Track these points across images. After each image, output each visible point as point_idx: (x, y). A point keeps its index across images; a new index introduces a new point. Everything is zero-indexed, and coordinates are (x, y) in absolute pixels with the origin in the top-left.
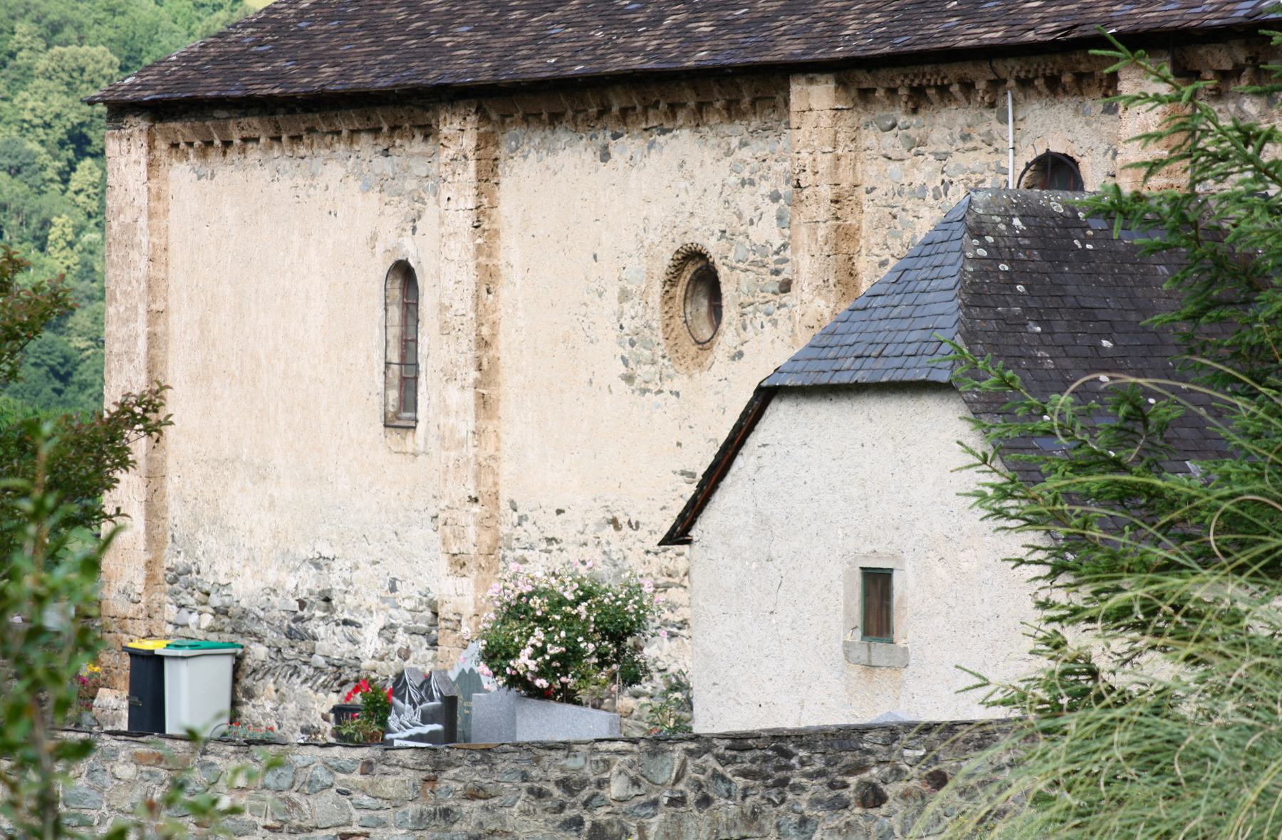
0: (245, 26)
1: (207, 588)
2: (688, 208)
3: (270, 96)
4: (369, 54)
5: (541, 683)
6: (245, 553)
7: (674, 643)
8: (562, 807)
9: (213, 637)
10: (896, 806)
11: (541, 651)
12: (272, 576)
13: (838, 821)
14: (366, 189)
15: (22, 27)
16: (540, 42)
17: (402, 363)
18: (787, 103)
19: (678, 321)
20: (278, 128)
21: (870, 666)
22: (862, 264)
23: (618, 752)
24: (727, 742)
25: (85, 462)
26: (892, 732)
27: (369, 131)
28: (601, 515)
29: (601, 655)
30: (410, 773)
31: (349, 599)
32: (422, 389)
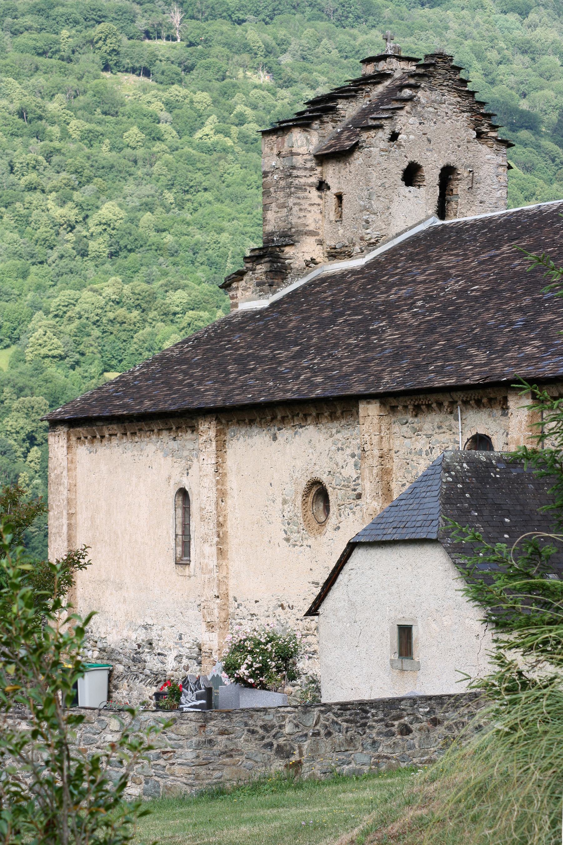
0: (110, 384)
1: (96, 639)
2: (313, 461)
3: (122, 415)
4: (166, 395)
5: (251, 681)
6: (113, 623)
7: (311, 661)
8: (263, 738)
9: (99, 662)
10: (416, 734)
11: (250, 666)
12: (125, 634)
13: (390, 742)
14: (166, 456)
15: (7, 389)
16: (244, 387)
17: (183, 534)
18: (358, 413)
19: (310, 513)
20: (125, 429)
21: (402, 670)
22: (393, 485)
23: (288, 712)
24: (339, 707)
25: (52, 582)
26: (414, 701)
27: (167, 429)
28: (275, 602)
29: (277, 667)
30: (193, 724)
31: (161, 643)
32: (192, 546)
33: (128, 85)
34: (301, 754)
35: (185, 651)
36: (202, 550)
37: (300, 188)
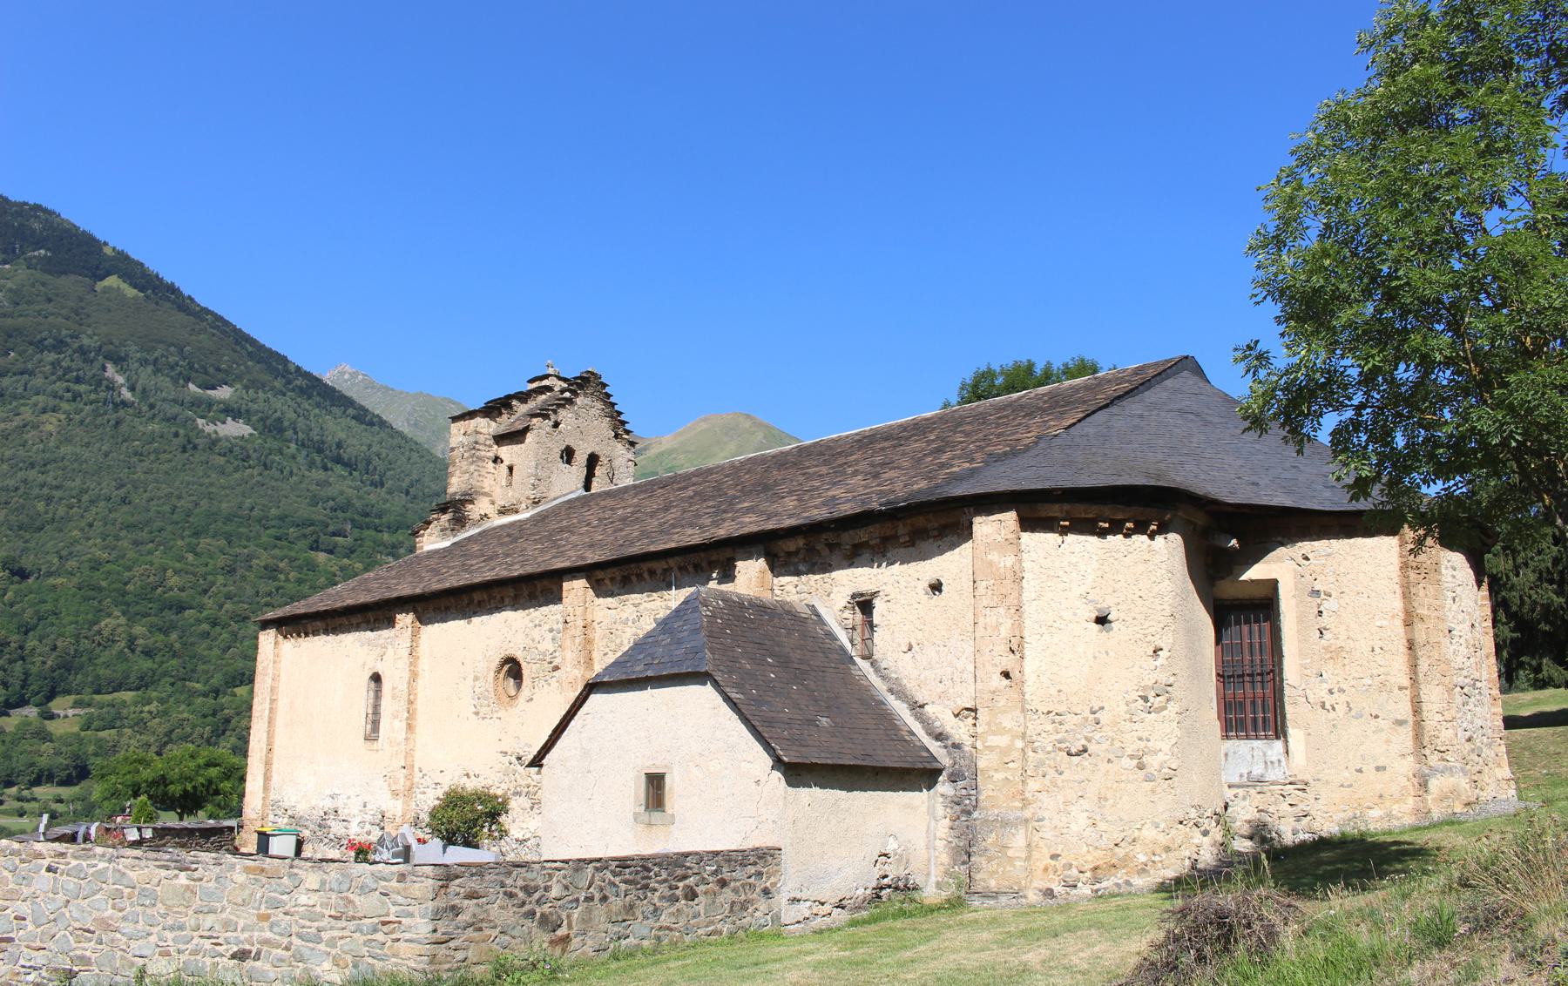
8: (523, 904)
12: (313, 803)
22: (595, 655)
33: (322, 557)
34: (570, 926)
35: (368, 818)
36: (391, 725)
37: (480, 459)
